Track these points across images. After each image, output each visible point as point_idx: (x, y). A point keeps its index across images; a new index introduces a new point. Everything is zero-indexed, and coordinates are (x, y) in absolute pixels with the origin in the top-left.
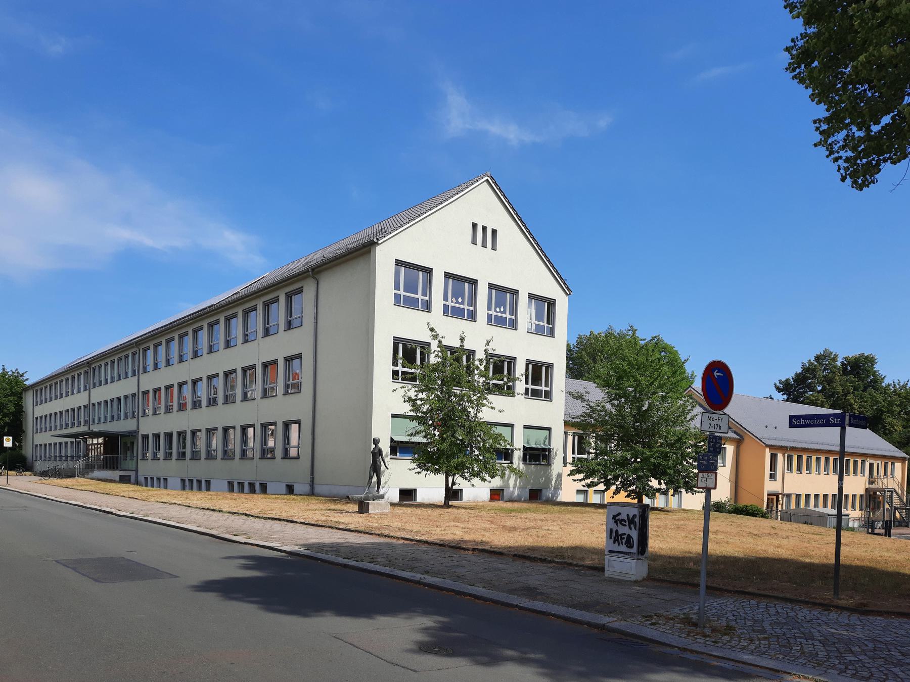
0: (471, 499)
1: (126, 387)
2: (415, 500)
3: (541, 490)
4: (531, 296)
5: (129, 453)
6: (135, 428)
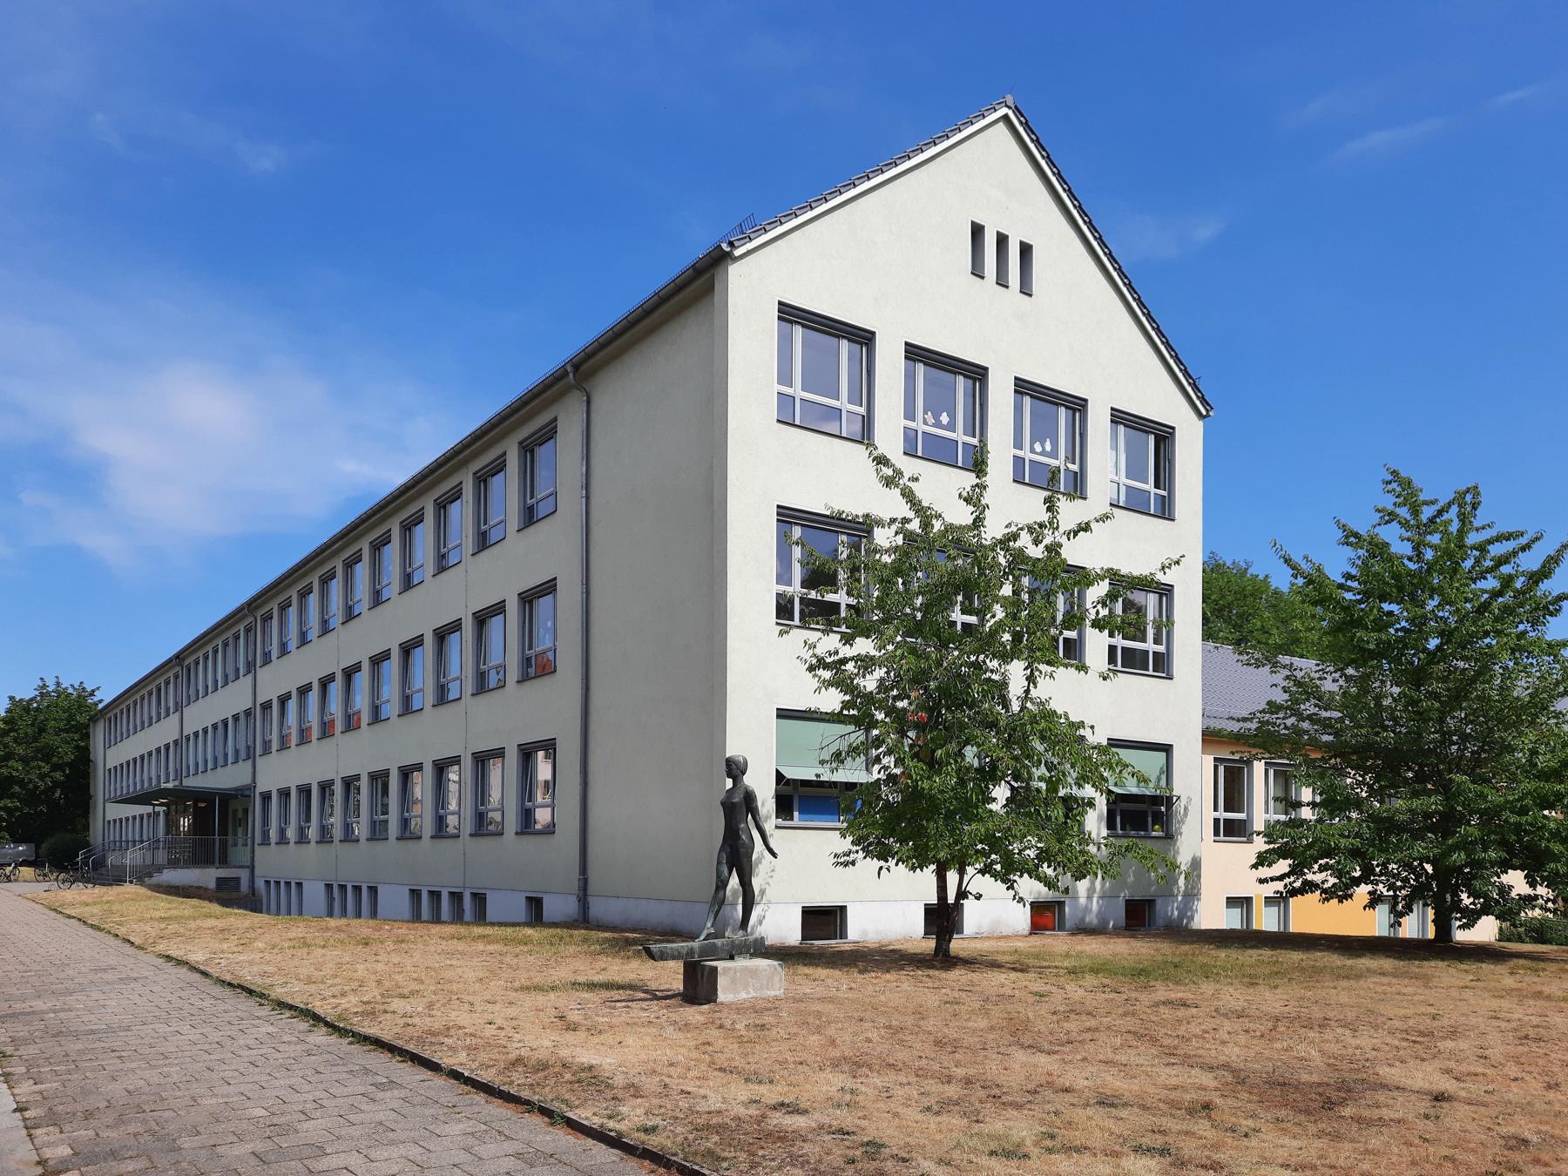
0: (985, 929)
1: (231, 700)
2: (843, 935)
3: (1151, 902)
4: (1119, 417)
5: (240, 830)
6: (247, 780)
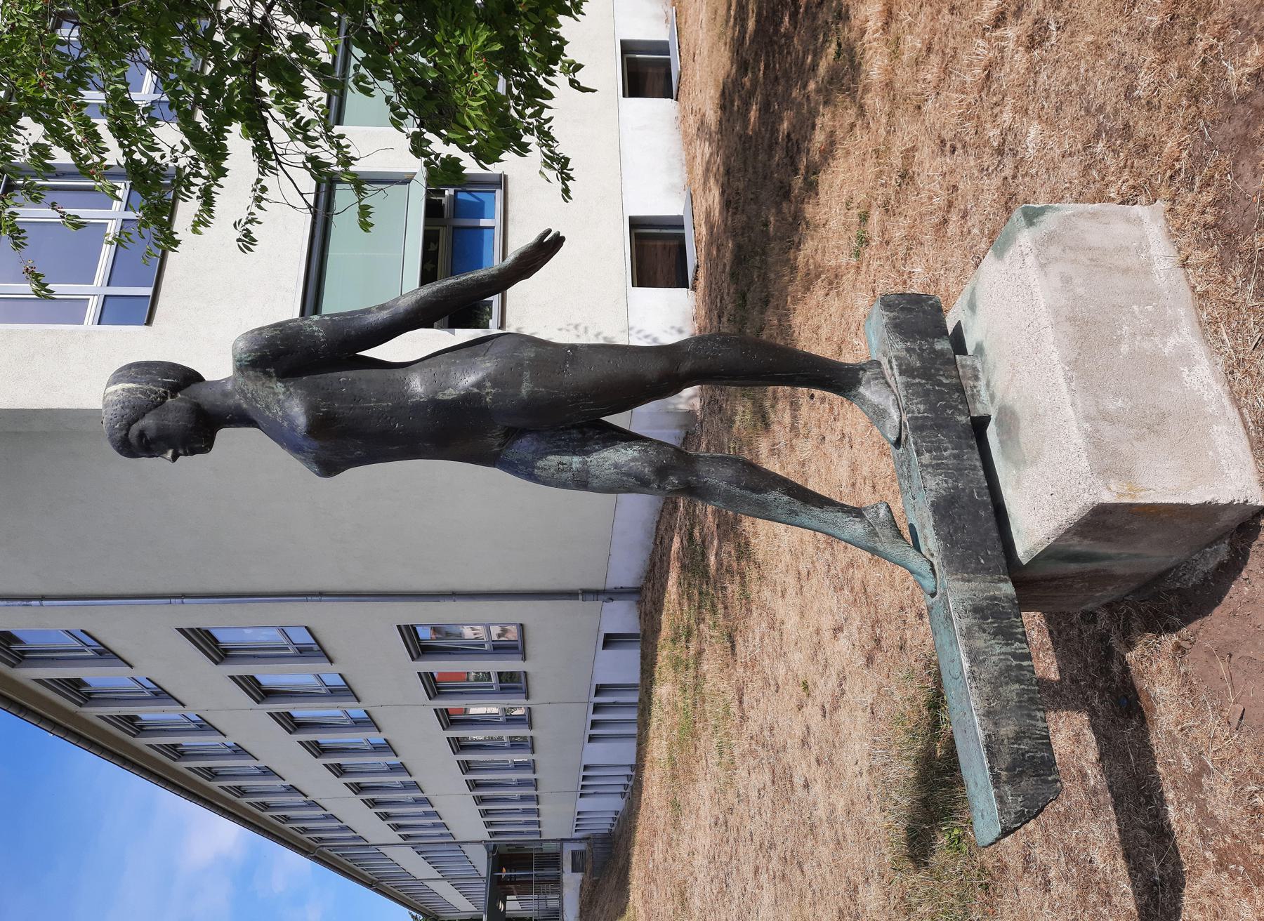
6: (482, 848)
